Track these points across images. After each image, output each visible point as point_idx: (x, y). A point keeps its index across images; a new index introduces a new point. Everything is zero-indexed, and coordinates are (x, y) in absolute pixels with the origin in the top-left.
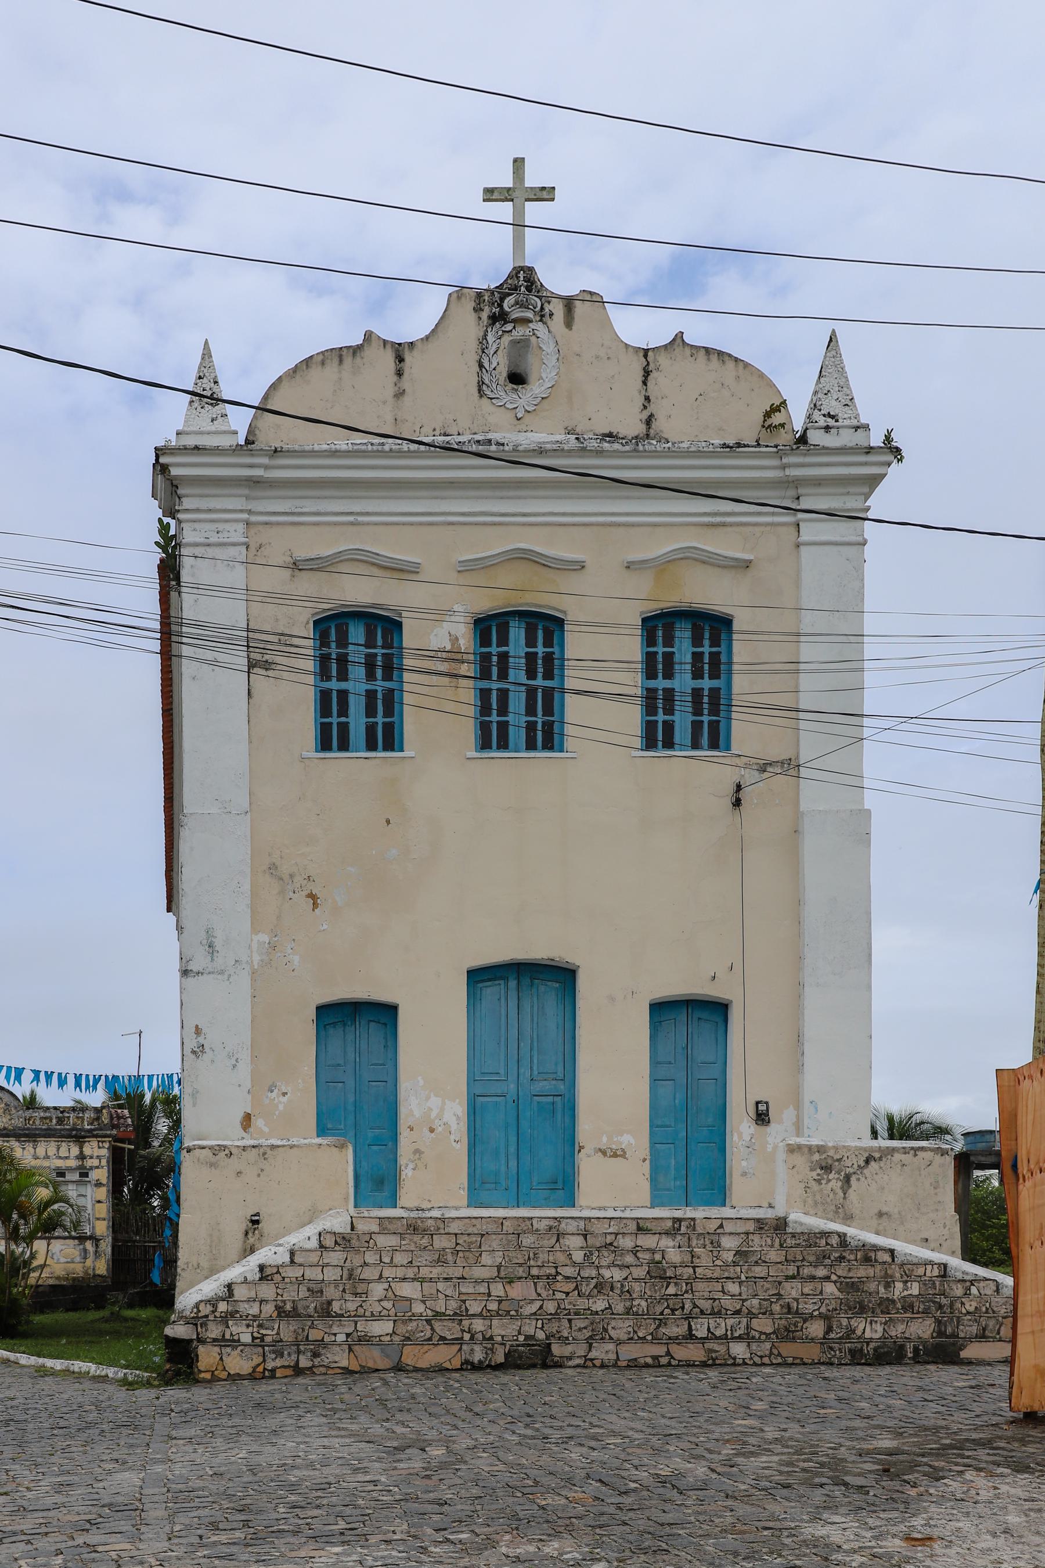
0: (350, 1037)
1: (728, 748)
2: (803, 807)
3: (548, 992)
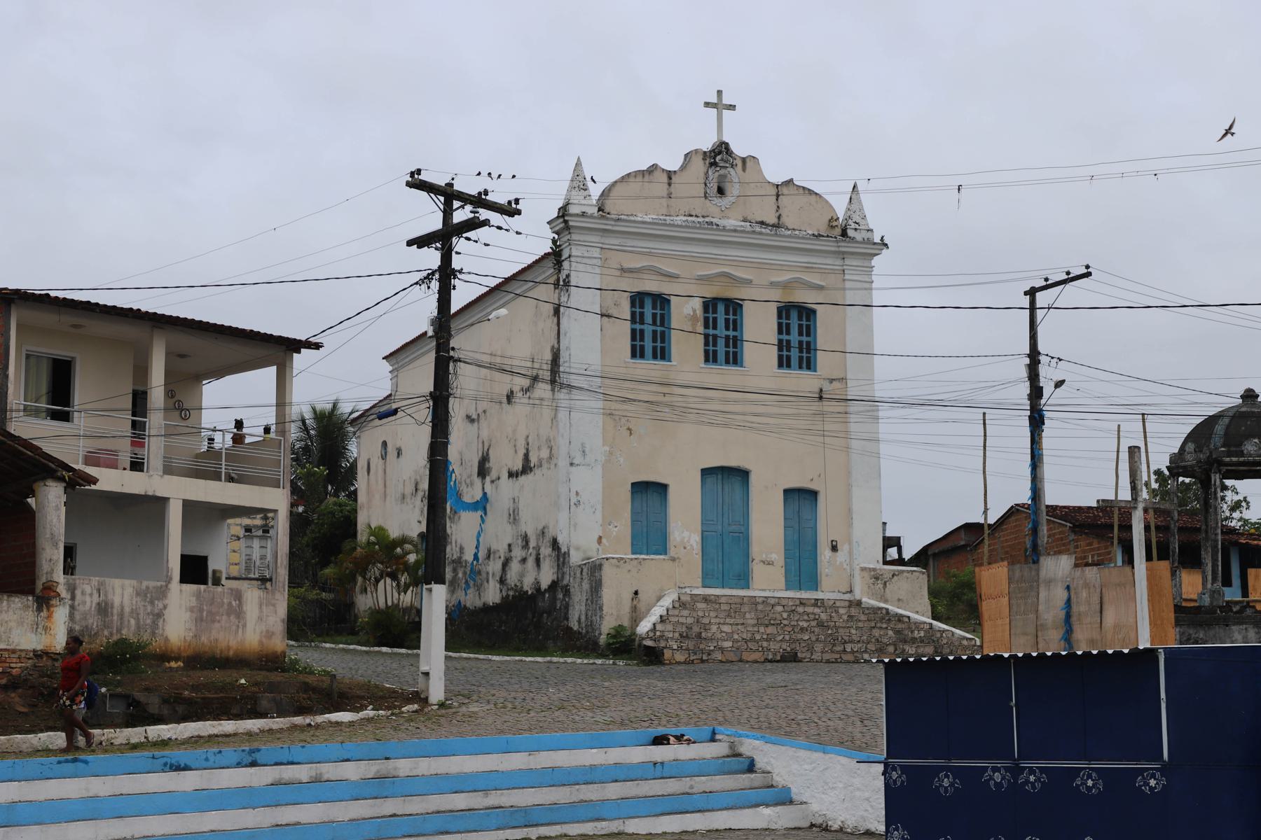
3: (736, 482)
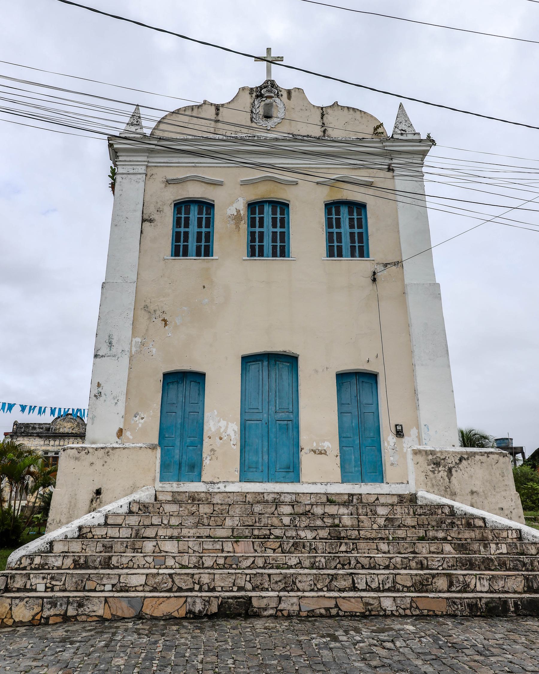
0: (181, 389)
1: (368, 257)
2: (407, 281)
3: (284, 368)
